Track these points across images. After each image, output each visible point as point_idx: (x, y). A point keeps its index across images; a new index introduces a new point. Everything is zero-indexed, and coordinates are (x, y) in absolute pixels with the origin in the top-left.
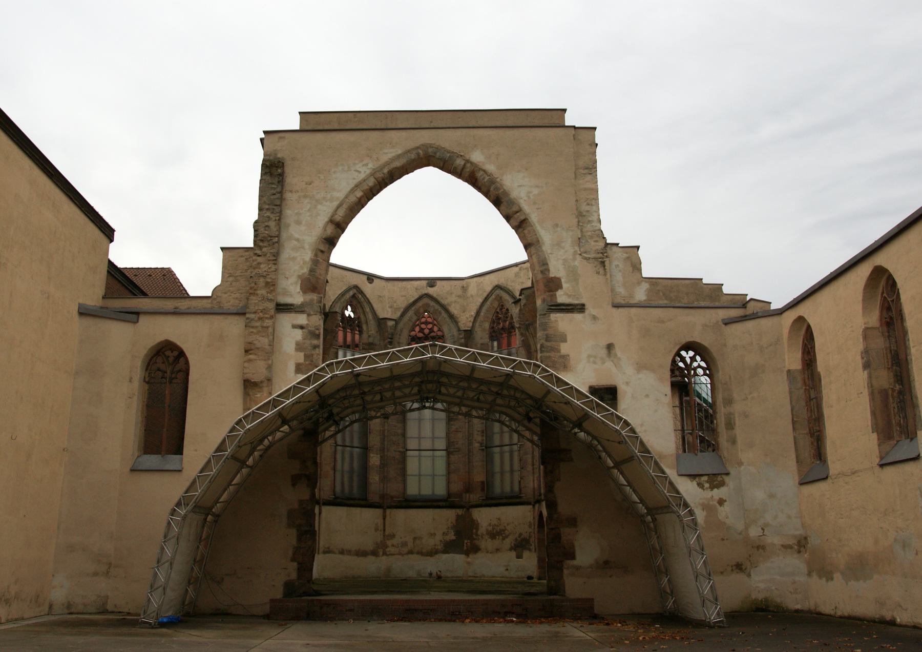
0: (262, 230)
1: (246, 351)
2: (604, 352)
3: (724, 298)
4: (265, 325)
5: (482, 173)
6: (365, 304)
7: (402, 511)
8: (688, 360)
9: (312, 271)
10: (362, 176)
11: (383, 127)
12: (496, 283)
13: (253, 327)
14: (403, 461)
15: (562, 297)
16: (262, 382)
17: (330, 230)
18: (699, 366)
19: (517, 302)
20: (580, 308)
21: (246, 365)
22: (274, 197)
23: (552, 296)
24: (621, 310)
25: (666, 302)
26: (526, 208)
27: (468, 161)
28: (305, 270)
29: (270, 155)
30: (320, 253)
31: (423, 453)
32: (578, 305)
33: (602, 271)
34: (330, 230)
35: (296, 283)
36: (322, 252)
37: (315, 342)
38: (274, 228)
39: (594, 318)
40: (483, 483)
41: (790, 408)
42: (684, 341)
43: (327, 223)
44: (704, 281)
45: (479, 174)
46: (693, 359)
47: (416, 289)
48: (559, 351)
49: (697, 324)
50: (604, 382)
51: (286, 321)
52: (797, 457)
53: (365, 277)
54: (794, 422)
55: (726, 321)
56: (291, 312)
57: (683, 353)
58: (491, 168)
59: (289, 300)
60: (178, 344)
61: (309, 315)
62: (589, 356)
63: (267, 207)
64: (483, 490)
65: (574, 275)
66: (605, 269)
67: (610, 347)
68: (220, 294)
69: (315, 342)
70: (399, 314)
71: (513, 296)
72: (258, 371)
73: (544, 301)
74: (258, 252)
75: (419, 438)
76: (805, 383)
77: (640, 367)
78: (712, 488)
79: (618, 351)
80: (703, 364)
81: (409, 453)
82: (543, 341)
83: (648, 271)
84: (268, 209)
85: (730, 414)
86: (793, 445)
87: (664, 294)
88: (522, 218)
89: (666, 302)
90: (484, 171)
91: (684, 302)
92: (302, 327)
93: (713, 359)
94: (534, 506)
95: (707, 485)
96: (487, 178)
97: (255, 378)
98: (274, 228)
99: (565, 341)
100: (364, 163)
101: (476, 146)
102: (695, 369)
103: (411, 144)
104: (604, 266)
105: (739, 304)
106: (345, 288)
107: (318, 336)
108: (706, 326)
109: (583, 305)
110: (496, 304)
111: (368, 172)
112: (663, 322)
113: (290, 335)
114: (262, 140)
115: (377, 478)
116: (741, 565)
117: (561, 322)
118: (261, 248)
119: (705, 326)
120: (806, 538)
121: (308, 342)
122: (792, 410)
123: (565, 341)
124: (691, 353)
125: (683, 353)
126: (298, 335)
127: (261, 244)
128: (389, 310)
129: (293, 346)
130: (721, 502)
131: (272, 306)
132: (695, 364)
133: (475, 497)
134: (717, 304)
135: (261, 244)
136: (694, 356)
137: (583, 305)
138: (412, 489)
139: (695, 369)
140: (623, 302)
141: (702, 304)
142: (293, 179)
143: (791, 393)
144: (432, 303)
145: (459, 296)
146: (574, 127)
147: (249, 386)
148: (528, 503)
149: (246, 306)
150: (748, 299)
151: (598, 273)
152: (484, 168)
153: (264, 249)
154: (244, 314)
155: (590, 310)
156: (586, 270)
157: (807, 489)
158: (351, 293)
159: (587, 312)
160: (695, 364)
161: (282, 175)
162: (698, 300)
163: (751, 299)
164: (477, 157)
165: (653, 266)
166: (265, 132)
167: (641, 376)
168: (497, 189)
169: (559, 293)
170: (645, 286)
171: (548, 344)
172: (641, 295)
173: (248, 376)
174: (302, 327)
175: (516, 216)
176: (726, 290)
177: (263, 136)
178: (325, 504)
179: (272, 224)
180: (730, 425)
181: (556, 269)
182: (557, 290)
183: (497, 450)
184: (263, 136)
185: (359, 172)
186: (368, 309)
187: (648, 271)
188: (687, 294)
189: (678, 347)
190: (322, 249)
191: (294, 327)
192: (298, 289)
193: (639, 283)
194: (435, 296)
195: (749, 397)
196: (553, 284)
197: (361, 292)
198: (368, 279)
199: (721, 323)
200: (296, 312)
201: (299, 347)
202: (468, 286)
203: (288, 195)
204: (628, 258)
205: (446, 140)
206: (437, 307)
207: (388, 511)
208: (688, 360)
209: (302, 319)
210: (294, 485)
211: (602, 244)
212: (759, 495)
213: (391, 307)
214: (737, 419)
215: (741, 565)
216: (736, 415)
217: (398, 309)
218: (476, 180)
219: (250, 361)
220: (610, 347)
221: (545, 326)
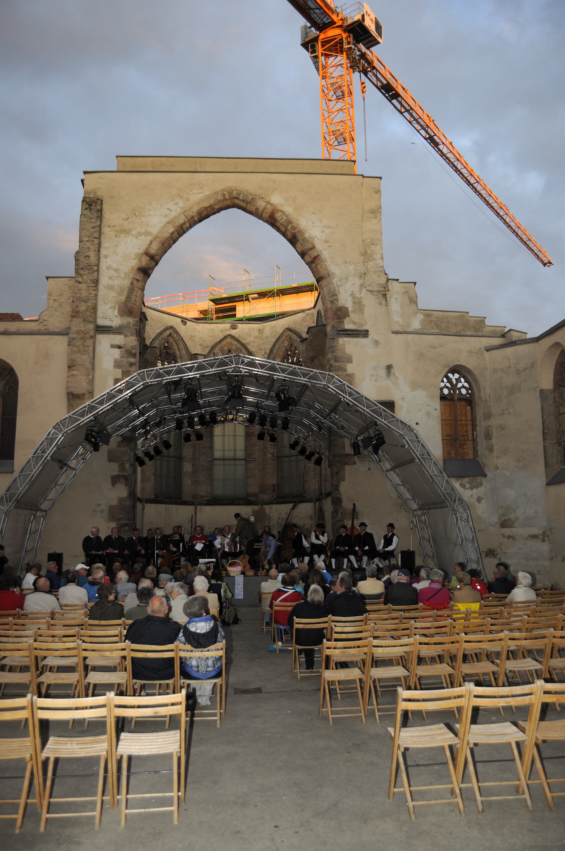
0: (82, 259)
1: (69, 367)
2: (383, 372)
3: (487, 329)
4: (86, 344)
5: (280, 213)
6: (180, 342)
7: (153, 505)
8: (454, 382)
9: (128, 297)
10: (174, 214)
11: (193, 170)
12: (287, 326)
13: (75, 346)
14: (210, 469)
15: (348, 325)
16: (84, 395)
17: (145, 261)
18: (463, 387)
19: (303, 340)
20: (365, 334)
21: (69, 379)
22: (94, 230)
23: (340, 322)
24: (399, 335)
25: (437, 331)
26: (319, 246)
27: (268, 203)
28: (123, 298)
29: (89, 193)
30: (135, 282)
31: (226, 462)
32: (362, 331)
33: (384, 302)
34: (145, 261)
35: (113, 308)
36: (138, 280)
37: (132, 360)
38: (93, 259)
39: (376, 343)
40: (274, 485)
41: (541, 422)
42: (452, 365)
43: (142, 255)
44: (470, 314)
45: (278, 216)
46: (458, 380)
47: (222, 331)
48: (345, 370)
49: (462, 350)
50: (385, 397)
51: (104, 342)
52: (546, 463)
53: (180, 320)
54: (544, 434)
55: (488, 348)
56: (109, 333)
57: (450, 375)
58: (288, 209)
59: (107, 323)
60: (8, 361)
61: (125, 336)
62: (372, 375)
63: (87, 239)
64: (274, 491)
65: (359, 305)
66: (386, 301)
67: (389, 368)
68: (45, 318)
69: (132, 360)
70: (207, 351)
71: (299, 336)
72: (81, 387)
73: (333, 327)
74: (80, 279)
75: (224, 436)
76: (555, 401)
77: (415, 386)
78: (472, 489)
79: (395, 370)
80: (466, 385)
81: (216, 462)
82: (332, 362)
83: (426, 301)
84: (88, 241)
85: (489, 426)
86: (543, 453)
87: (436, 325)
88: (316, 254)
89: (437, 331)
90: (282, 212)
91: (453, 330)
92: (119, 347)
93: (476, 380)
94: (315, 503)
95: (468, 486)
96: (285, 218)
97: (78, 391)
98: (93, 259)
99: (351, 362)
100: (175, 202)
101: (275, 189)
102: (459, 389)
103: (219, 187)
104: (386, 298)
105: (499, 335)
106: (163, 328)
107: (134, 355)
108: (472, 352)
109: (367, 331)
110: (286, 344)
111: (179, 210)
112: (435, 348)
113: (108, 354)
114: (82, 181)
115: (190, 482)
116: (494, 551)
117: (348, 345)
118: (82, 276)
119: (470, 352)
120: (550, 530)
121: (125, 360)
122: (543, 423)
123: (351, 362)
124: (457, 376)
125: (450, 375)
126: (117, 353)
127: (81, 272)
128: (200, 347)
129: (112, 364)
130: (479, 500)
131: (91, 326)
132: (460, 385)
133: (265, 497)
134: (480, 334)
135: (81, 272)
136: (459, 378)
137: (367, 331)
138: (219, 491)
139: (459, 389)
140: (401, 330)
141: (468, 333)
142: (111, 216)
143: (542, 409)
144: (235, 342)
145: (256, 337)
146: (363, 176)
147: (73, 397)
148: (310, 501)
149: (69, 328)
150: (506, 330)
151: (381, 304)
152: (282, 209)
153: (85, 277)
154: (67, 334)
155: (372, 335)
156: (371, 303)
157: (554, 489)
158: (168, 332)
159: (370, 337)
160: (460, 385)
161: (101, 211)
162: (464, 331)
163: (510, 330)
164: (276, 199)
165: (430, 299)
166: (85, 173)
167: (415, 393)
168: (294, 228)
169: (346, 321)
170: (420, 317)
171: (336, 364)
172: (416, 324)
173: (72, 390)
174: (119, 347)
175: (310, 253)
176: (487, 322)
177: (83, 176)
178: (147, 502)
179: (92, 254)
180: (488, 436)
181: (345, 300)
182: (345, 318)
183: (286, 459)
184: (83, 176)
185: (171, 210)
186: (182, 346)
187: (426, 301)
188: (456, 325)
189: (447, 369)
190: (138, 278)
191: (113, 346)
192: (116, 312)
193: (415, 314)
194: (237, 336)
195: (506, 413)
196: (341, 313)
197: (177, 332)
198: (182, 321)
199: (483, 350)
200: (115, 333)
201: (117, 364)
202: (263, 330)
203: (105, 230)
204: (406, 292)
205: (248, 184)
206: (239, 345)
207: (198, 507)
208: (454, 382)
209: (119, 339)
210: (113, 484)
211: (383, 280)
212: (511, 494)
213: (201, 345)
214: (494, 431)
215: (494, 551)
216: (494, 428)
217: (207, 347)
218: (276, 220)
219: (73, 375)
220: (389, 368)
221: (333, 349)
